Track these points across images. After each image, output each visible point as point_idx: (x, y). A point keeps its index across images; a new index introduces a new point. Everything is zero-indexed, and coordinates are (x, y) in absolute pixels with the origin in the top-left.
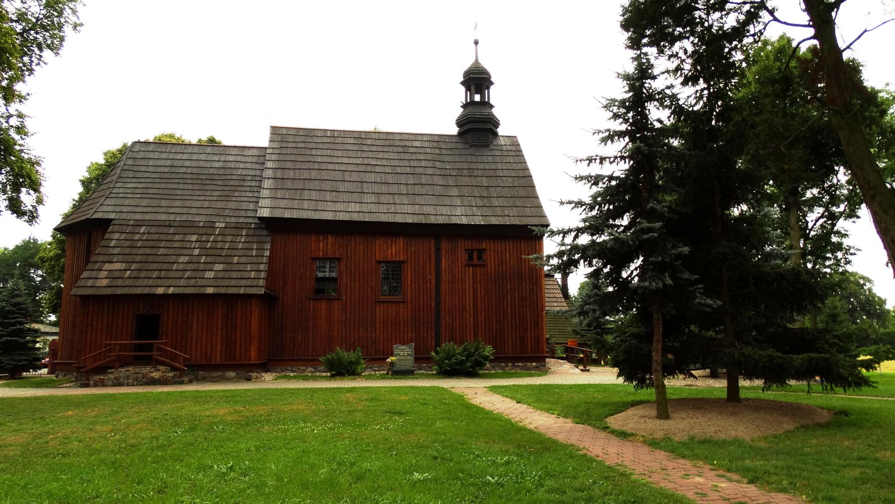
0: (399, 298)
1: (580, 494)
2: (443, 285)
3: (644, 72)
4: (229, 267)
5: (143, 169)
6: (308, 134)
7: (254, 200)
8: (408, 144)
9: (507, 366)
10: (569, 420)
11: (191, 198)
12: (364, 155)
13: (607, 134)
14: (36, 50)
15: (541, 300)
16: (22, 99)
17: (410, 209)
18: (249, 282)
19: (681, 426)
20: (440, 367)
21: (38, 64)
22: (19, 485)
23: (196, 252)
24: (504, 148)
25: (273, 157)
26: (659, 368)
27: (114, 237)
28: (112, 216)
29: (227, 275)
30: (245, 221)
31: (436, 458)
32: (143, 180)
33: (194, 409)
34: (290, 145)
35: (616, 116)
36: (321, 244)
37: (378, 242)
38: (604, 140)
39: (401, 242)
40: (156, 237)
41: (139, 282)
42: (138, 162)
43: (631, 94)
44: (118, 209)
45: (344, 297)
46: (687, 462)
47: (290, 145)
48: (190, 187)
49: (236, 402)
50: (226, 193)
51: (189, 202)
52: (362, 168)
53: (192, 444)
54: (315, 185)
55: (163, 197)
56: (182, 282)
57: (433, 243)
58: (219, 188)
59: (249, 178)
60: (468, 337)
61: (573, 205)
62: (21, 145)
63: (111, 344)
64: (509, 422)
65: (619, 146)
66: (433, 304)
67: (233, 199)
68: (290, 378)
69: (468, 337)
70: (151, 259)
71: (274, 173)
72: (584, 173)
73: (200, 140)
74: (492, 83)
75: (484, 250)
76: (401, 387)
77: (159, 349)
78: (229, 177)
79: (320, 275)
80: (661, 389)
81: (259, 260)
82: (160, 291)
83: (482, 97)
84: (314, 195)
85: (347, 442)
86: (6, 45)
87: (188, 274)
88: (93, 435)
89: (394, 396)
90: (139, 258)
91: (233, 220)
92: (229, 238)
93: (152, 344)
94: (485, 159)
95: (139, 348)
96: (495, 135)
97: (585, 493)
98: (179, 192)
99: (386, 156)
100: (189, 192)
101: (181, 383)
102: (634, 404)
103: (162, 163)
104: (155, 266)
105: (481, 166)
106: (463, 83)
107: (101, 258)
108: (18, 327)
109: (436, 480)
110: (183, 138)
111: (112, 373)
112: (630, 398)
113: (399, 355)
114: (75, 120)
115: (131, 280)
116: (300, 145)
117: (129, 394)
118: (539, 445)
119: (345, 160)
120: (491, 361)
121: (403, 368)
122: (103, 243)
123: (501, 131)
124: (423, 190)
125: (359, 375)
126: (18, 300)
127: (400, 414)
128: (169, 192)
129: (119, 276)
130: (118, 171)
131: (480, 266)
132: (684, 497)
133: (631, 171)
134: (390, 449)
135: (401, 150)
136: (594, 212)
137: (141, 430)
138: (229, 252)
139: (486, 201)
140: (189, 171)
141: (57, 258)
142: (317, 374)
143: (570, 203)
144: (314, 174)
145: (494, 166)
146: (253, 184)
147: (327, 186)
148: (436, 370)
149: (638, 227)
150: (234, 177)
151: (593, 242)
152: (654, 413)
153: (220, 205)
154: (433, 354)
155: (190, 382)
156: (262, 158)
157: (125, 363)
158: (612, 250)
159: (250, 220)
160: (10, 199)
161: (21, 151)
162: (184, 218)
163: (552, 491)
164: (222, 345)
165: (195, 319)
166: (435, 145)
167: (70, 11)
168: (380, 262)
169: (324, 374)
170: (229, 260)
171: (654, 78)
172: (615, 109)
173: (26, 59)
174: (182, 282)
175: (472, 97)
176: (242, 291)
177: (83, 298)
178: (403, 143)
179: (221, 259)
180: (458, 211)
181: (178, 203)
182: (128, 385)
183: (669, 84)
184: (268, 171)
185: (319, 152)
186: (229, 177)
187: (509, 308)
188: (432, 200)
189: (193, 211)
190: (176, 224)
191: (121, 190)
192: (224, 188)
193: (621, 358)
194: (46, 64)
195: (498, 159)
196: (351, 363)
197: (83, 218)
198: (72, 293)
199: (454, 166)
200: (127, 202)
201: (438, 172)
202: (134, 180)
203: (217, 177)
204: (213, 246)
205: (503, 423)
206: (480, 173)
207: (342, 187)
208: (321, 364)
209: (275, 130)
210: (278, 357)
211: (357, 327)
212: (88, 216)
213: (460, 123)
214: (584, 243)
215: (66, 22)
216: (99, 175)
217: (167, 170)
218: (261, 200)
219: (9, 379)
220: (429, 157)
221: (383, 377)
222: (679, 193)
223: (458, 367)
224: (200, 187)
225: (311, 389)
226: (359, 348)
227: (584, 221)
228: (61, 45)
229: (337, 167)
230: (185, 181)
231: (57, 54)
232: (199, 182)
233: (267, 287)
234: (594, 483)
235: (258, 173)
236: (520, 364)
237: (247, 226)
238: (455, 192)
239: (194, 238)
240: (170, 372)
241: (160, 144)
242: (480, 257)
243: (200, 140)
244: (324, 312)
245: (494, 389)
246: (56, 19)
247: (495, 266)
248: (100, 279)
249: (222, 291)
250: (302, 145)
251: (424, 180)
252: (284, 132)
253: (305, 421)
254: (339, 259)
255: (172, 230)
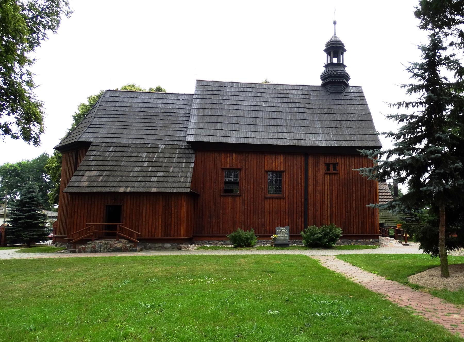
0: (280, 196)
1: (374, 325)
2: (310, 187)
3: (436, 45)
4: (167, 174)
5: (112, 108)
6: (221, 85)
7: (184, 129)
8: (287, 92)
9: (352, 241)
10: (384, 278)
11: (143, 128)
12: (258, 99)
13: (411, 87)
14: (42, 29)
15: (376, 197)
16: (30, 62)
17: (288, 136)
18: (179, 185)
19: (455, 282)
20: (307, 242)
21: (43, 39)
22: (17, 315)
23: (146, 164)
24: (353, 95)
25: (198, 101)
26: (443, 243)
27: (93, 154)
28: (91, 140)
29: (166, 179)
30: (178, 143)
31: (287, 301)
32: (112, 116)
33: (140, 268)
34: (209, 93)
35: (416, 75)
36: (228, 159)
37: (266, 158)
38: (410, 91)
39: (281, 158)
40: (119, 154)
41: (108, 184)
42: (109, 104)
43: (427, 60)
44: (95, 135)
45: (243, 195)
46: (453, 305)
47: (209, 93)
48: (143, 121)
49: (168, 264)
50: (166, 125)
51: (142, 131)
52: (257, 108)
53: (132, 290)
54: (225, 120)
55: (125, 127)
56: (136, 184)
57: (303, 159)
58: (162, 121)
59: (182, 115)
60: (326, 222)
61: (386, 135)
62: (29, 93)
63: (90, 225)
64: (344, 279)
65: (422, 95)
66: (303, 200)
67: (171, 129)
68: (207, 248)
69: (326, 222)
70: (116, 168)
71: (198, 112)
72: (394, 113)
73: (151, 89)
74: (345, 51)
75: (338, 163)
76: (278, 255)
77: (121, 228)
78: (169, 114)
79: (227, 180)
80: (444, 257)
81: (187, 170)
82: (122, 190)
83: (339, 60)
84: (224, 126)
85: (232, 290)
86: (19, 27)
87: (140, 179)
88: (72, 284)
89: (272, 261)
90: (108, 168)
91: (171, 143)
92: (167, 155)
93: (116, 225)
94: (339, 102)
95: (108, 227)
96: (347, 85)
97: (377, 324)
98: (135, 124)
99: (273, 100)
100: (142, 124)
101: (135, 251)
102: (430, 267)
103: (124, 104)
104: (118, 173)
105: (337, 107)
106: (325, 51)
107: (84, 168)
108: (32, 213)
109: (282, 314)
110: (140, 88)
111: (90, 243)
112: (430, 263)
113: (279, 233)
114: (64, 77)
115: (103, 183)
116: (215, 93)
117: (100, 258)
118: (360, 293)
119: (245, 103)
120: (341, 238)
121: (282, 242)
122: (85, 158)
123: (350, 83)
124: (297, 123)
125: (253, 246)
126: (32, 195)
127: (273, 272)
128: (129, 124)
129: (95, 180)
130: (96, 110)
131: (335, 174)
132: (443, 328)
133: (428, 112)
134: (258, 296)
135: (283, 96)
136: (401, 140)
137: (102, 281)
138: (168, 164)
139: (339, 131)
140: (142, 110)
141: (57, 167)
142: (225, 246)
143: (384, 133)
144: (224, 112)
145: (345, 107)
146: (184, 119)
147: (233, 120)
148: (305, 243)
149: (429, 150)
150: (172, 114)
151: (399, 159)
152: (439, 273)
153: (162, 133)
154: (302, 233)
155: (141, 250)
156: (190, 102)
157: (100, 237)
158: (410, 164)
159: (181, 143)
160: (23, 129)
161: (29, 98)
162: (138, 141)
163: (357, 322)
164: (162, 226)
165: (145, 209)
166: (306, 92)
167: (64, 3)
168: (267, 172)
169: (230, 246)
170: (167, 169)
171: (444, 49)
172: (416, 71)
173: (35, 35)
174: (136, 184)
175: (331, 60)
176: (175, 190)
177: (73, 195)
178: (284, 92)
179: (162, 169)
180: (320, 137)
181: (134, 132)
182: (101, 252)
183: (452, 54)
184: (194, 110)
185: (228, 98)
186: (169, 114)
187: (354, 203)
188: (303, 130)
189: (144, 137)
190: (133, 145)
191: (98, 123)
192: (165, 122)
193: (420, 236)
194: (47, 38)
195: (348, 102)
196: (248, 239)
197: (73, 141)
198: (64, 191)
199: (318, 107)
200: (101, 130)
201: (307, 111)
202: (106, 116)
203: (160, 114)
204: (157, 160)
205: (338, 279)
206: (336, 111)
207: (242, 121)
208: (228, 239)
209: (199, 83)
210: (199, 234)
211: (252, 214)
212: (75, 140)
213: (323, 77)
214: (392, 161)
215: (61, 11)
216: (85, 112)
217: (127, 109)
218: (188, 130)
219: (27, 247)
220: (301, 101)
221: (268, 248)
222: (460, 126)
223: (319, 242)
224: (149, 121)
225: (218, 256)
226: (252, 229)
227: (396, 145)
228: (58, 26)
229: (240, 108)
230: (139, 117)
231: (55, 32)
232: (148, 117)
233: (192, 188)
234: (385, 318)
235: (187, 112)
236: (362, 240)
237: (179, 147)
238: (318, 124)
239: (144, 155)
240: (128, 243)
241: (125, 91)
242: (335, 169)
243: (151, 89)
244: (230, 205)
245: (340, 257)
246: (54, 9)
247: (345, 175)
248: (83, 182)
249: (162, 190)
250: (217, 93)
251: (298, 116)
252: (205, 84)
253: (209, 277)
254: (240, 169)
255: (130, 150)
